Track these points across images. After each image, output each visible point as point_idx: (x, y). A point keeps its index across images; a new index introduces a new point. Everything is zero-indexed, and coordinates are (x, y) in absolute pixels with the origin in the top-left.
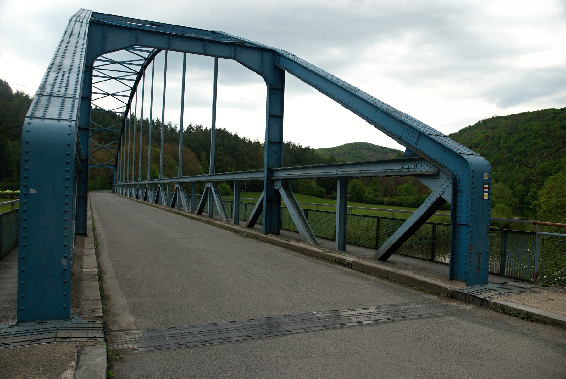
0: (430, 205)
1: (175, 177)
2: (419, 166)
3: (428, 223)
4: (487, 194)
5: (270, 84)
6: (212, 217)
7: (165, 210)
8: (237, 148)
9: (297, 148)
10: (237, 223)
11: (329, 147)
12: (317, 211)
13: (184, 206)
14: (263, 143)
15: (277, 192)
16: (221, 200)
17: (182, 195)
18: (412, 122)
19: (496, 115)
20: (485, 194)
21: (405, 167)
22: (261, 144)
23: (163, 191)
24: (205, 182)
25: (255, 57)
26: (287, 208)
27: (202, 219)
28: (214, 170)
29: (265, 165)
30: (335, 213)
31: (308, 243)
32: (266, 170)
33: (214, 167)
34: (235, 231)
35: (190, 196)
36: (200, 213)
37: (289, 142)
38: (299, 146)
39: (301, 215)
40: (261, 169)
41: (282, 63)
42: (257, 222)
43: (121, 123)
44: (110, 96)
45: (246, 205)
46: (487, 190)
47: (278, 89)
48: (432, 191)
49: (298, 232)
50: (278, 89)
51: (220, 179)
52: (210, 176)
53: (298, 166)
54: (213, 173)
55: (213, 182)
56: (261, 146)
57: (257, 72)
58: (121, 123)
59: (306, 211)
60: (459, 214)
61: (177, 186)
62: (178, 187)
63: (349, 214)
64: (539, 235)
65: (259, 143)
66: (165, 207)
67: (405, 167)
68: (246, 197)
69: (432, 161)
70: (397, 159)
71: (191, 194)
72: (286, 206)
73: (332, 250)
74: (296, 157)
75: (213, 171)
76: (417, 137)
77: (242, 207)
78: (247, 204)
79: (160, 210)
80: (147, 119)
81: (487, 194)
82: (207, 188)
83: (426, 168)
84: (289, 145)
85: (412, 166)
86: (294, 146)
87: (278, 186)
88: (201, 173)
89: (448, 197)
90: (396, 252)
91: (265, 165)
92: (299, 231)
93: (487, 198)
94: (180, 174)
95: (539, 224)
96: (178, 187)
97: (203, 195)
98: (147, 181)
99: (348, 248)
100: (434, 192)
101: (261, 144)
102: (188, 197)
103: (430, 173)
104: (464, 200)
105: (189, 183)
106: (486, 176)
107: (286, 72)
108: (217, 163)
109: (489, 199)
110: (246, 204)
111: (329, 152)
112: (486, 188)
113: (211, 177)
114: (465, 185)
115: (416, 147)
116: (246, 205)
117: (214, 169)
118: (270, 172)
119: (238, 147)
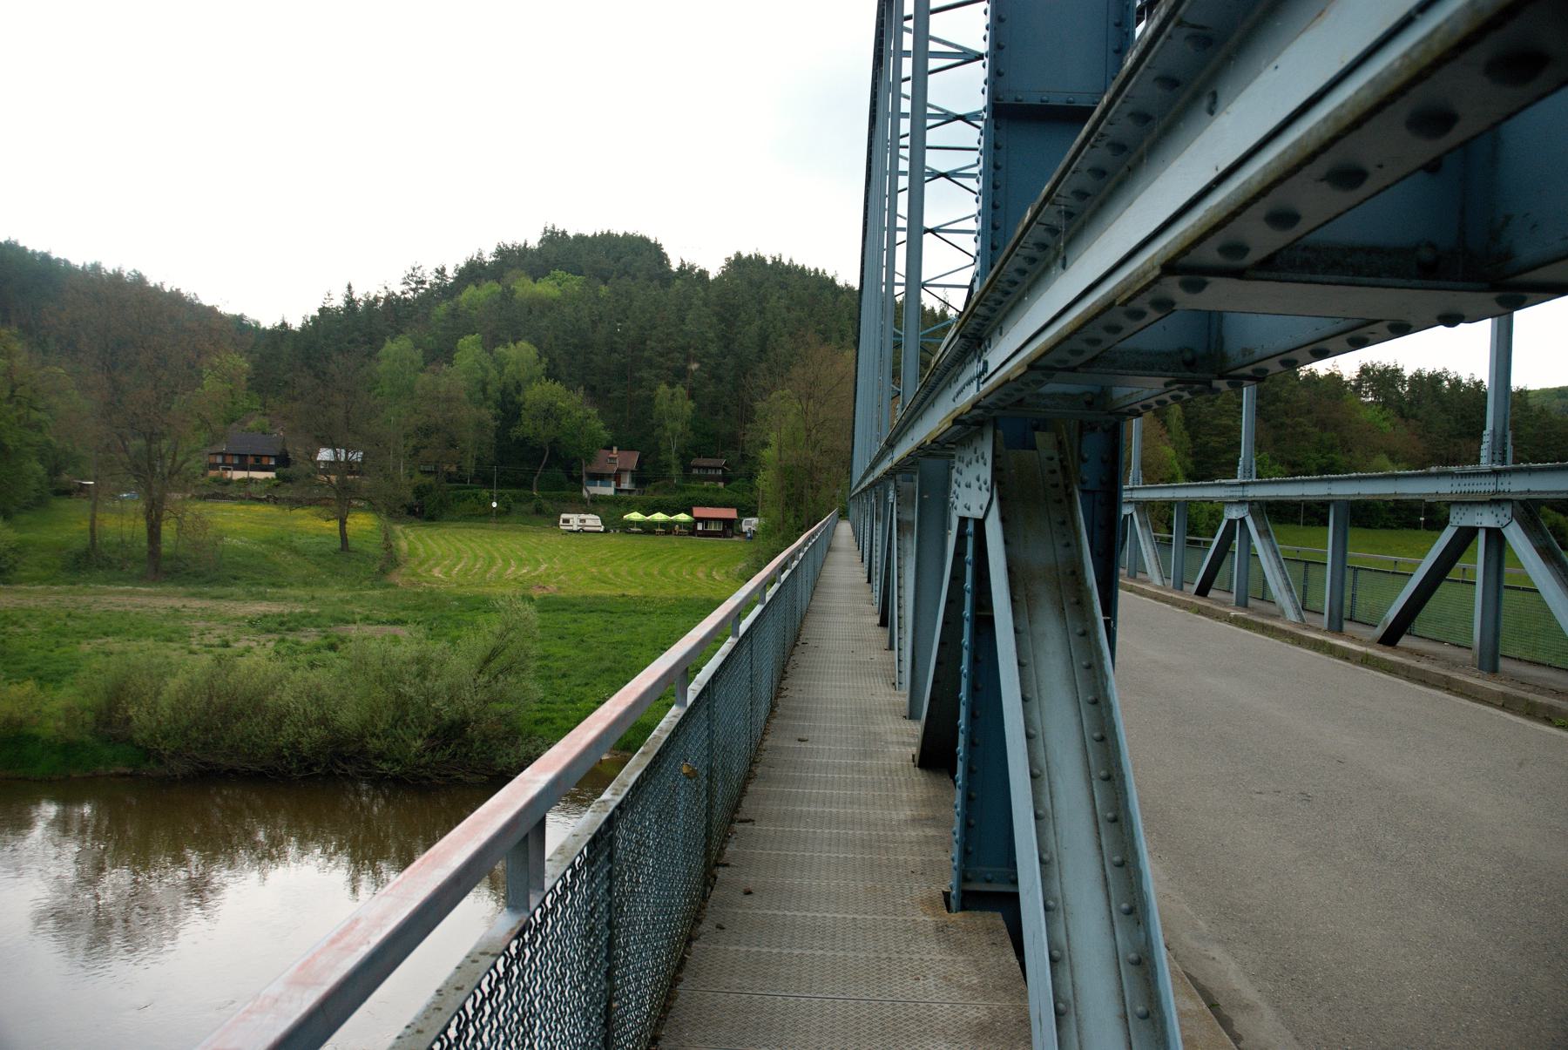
1: (1223, 481)
6: (1135, 577)
7: (1156, 597)
8: (1277, 393)
9: (1468, 389)
10: (1336, 627)
11: (1557, 386)
13: (1149, 571)
14: (1354, 376)
16: (1278, 557)
17: (1143, 536)
22: (1345, 379)
23: (1145, 530)
24: (1449, 504)
26: (1537, 591)
27: (1455, 680)
28: (1509, 448)
30: (1474, 583)
33: (1509, 434)
34: (1175, 603)
35: (1171, 539)
36: (1203, 591)
37: (1438, 371)
38: (1475, 383)
42: (1214, 586)
44: (942, 179)
51: (1303, 495)
52: (1243, 484)
53: (1354, 474)
54: (1503, 461)
55: (1251, 503)
56: (1346, 386)
61: (1234, 513)
62: (1131, 515)
65: (1340, 378)
66: (1291, 623)
68: (1367, 551)
71: (1174, 536)
72: (1533, 583)
73: (1225, 604)
74: (1463, 417)
75: (1505, 452)
77: (1349, 575)
78: (1359, 571)
79: (1168, 606)
82: (1231, 523)
84: (1441, 381)
86: (1457, 383)
88: (1174, 478)
92: (1276, 600)
94: (1248, 467)
96: (1242, 520)
97: (1216, 541)
99: (1347, 626)
101: (1345, 379)
102: (1163, 544)
105: (1170, 504)
108: (1216, 439)
110: (1307, 563)
111: (1557, 400)
113: (1246, 489)
117: (1509, 441)
119: (1278, 389)
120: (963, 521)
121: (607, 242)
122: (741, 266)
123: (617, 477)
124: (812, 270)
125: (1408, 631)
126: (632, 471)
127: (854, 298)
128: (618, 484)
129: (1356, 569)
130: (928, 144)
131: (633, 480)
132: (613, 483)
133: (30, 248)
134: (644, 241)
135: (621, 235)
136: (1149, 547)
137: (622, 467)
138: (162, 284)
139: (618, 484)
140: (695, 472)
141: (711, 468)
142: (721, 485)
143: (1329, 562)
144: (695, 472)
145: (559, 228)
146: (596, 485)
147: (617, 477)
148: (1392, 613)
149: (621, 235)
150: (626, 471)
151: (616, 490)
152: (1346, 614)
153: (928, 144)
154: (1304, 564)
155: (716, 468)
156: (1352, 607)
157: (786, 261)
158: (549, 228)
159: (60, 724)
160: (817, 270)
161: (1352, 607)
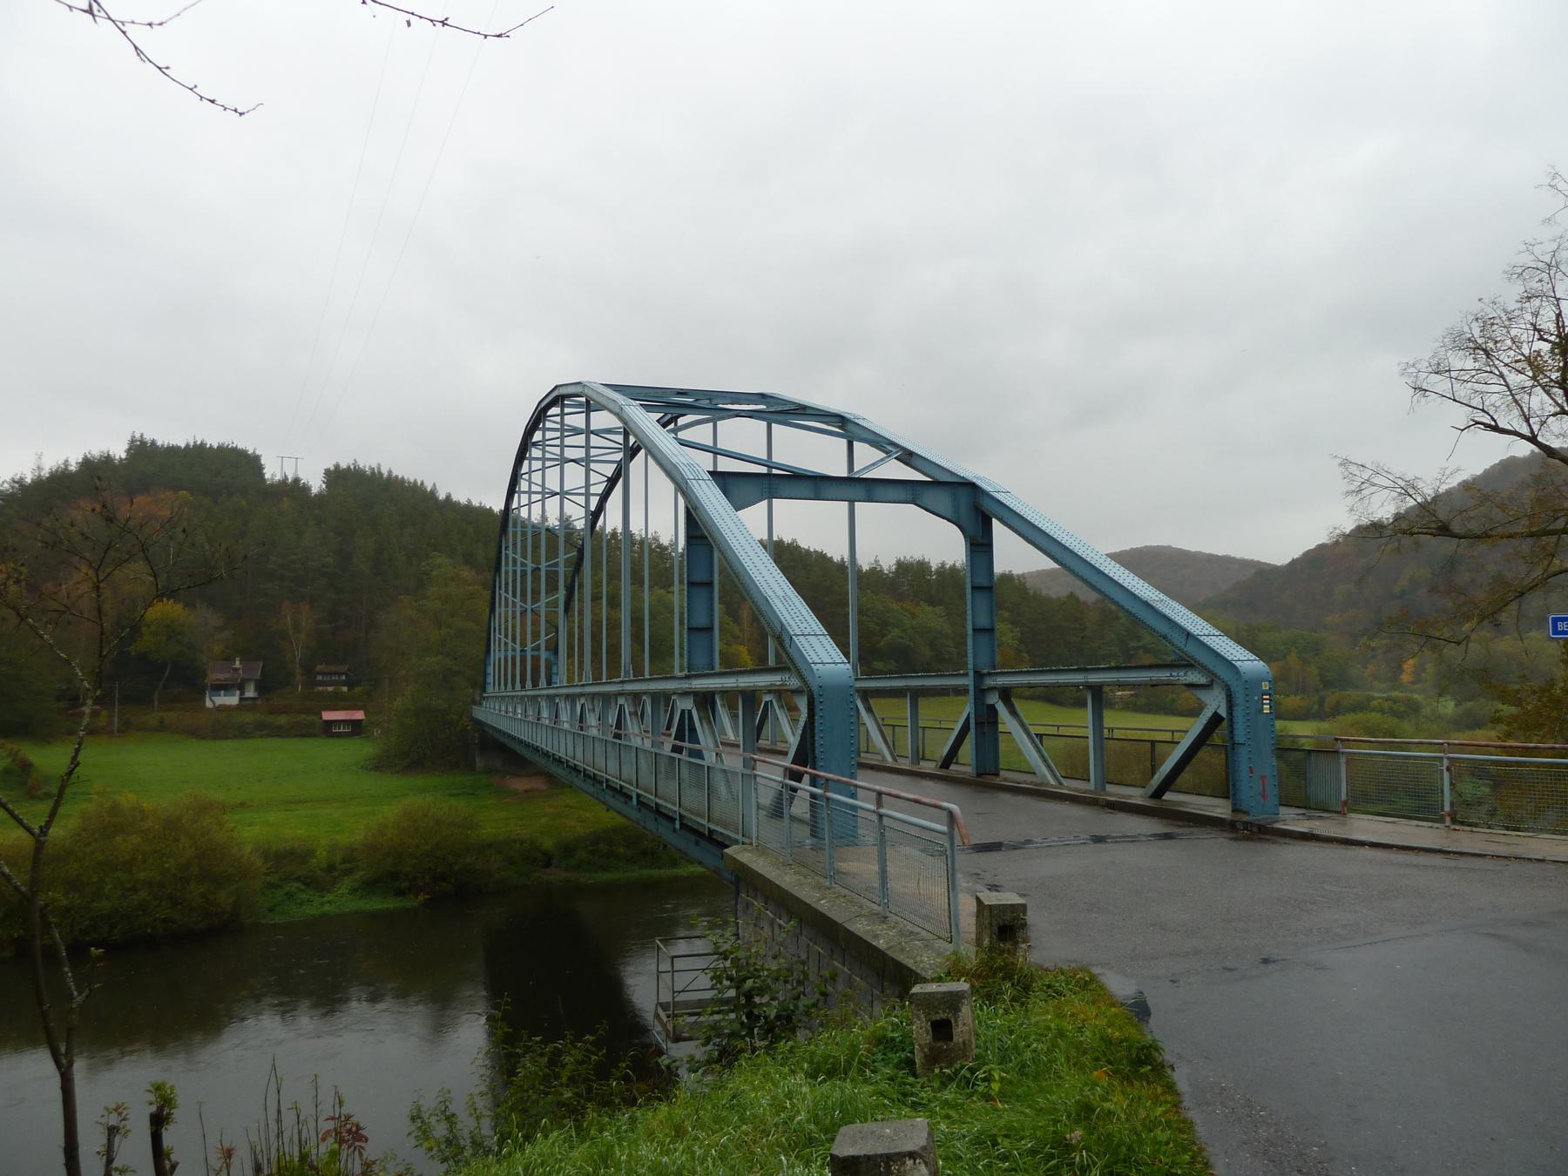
0: (1205, 722)
2: (1189, 673)
3: (1209, 745)
4: (1268, 706)
5: (970, 537)
12: (1058, 736)
15: (992, 710)
18: (1179, 618)
19: (1474, 473)
20: (1265, 706)
21: (1173, 674)
23: (782, 712)
25: (942, 499)
29: (970, 666)
31: (948, 974)
32: (971, 673)
39: (1033, 742)
40: (962, 672)
41: (987, 505)
43: (575, 553)
45: (894, 728)
46: (1268, 702)
47: (983, 545)
48: (1206, 705)
49: (1035, 773)
50: (983, 545)
57: (949, 520)
58: (575, 553)
59: (1040, 736)
60: (1236, 732)
61: (767, 698)
63: (1107, 738)
64: (1343, 753)
67: (1173, 674)
69: (1205, 670)
70: (865, 937)
76: (1185, 637)
80: (614, 530)
81: (1268, 706)
82: (766, 703)
83: (1199, 676)
85: (1182, 674)
87: (993, 699)
89: (1223, 712)
90: (1172, 788)
91: (970, 666)
92: (1035, 771)
93: (1268, 711)
95: (1342, 740)
96: (771, 701)
98: (622, 682)
100: (1208, 706)
102: (734, 717)
103: (1202, 683)
104: (1239, 712)
106: (1265, 686)
107: (994, 521)
109: (1271, 713)
112: (1267, 699)
114: (1239, 698)
115: (1185, 649)
116: (924, 730)
118: (979, 676)
120: (683, 711)
121: (198, 454)
122: (338, 477)
123: (241, 687)
124: (412, 481)
125: (954, 761)
126: (256, 680)
127: (841, 566)
128: (242, 693)
129: (924, 728)
130: (592, 445)
131: (259, 688)
132: (238, 692)
133: (1279, 564)
134: (235, 450)
135: (215, 446)
136: (727, 719)
137: (246, 676)
138: (923, 556)
139: (242, 693)
140: (319, 678)
141: (335, 674)
142: (345, 689)
143: (909, 725)
144: (319, 678)
145: (148, 437)
146: (220, 695)
147: (242, 688)
148: (946, 750)
149: (215, 446)
150: (250, 680)
151: (241, 699)
152: (921, 757)
153: (592, 445)
154: (891, 728)
155: (340, 674)
156: (923, 753)
157: (385, 472)
158: (138, 436)
159: (953, 1055)
160: (415, 480)
161: (923, 753)
